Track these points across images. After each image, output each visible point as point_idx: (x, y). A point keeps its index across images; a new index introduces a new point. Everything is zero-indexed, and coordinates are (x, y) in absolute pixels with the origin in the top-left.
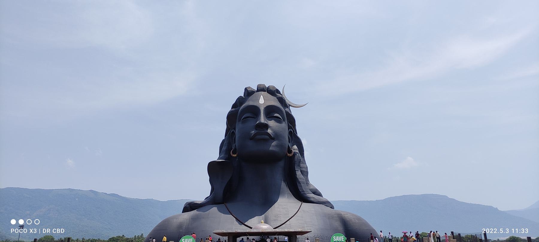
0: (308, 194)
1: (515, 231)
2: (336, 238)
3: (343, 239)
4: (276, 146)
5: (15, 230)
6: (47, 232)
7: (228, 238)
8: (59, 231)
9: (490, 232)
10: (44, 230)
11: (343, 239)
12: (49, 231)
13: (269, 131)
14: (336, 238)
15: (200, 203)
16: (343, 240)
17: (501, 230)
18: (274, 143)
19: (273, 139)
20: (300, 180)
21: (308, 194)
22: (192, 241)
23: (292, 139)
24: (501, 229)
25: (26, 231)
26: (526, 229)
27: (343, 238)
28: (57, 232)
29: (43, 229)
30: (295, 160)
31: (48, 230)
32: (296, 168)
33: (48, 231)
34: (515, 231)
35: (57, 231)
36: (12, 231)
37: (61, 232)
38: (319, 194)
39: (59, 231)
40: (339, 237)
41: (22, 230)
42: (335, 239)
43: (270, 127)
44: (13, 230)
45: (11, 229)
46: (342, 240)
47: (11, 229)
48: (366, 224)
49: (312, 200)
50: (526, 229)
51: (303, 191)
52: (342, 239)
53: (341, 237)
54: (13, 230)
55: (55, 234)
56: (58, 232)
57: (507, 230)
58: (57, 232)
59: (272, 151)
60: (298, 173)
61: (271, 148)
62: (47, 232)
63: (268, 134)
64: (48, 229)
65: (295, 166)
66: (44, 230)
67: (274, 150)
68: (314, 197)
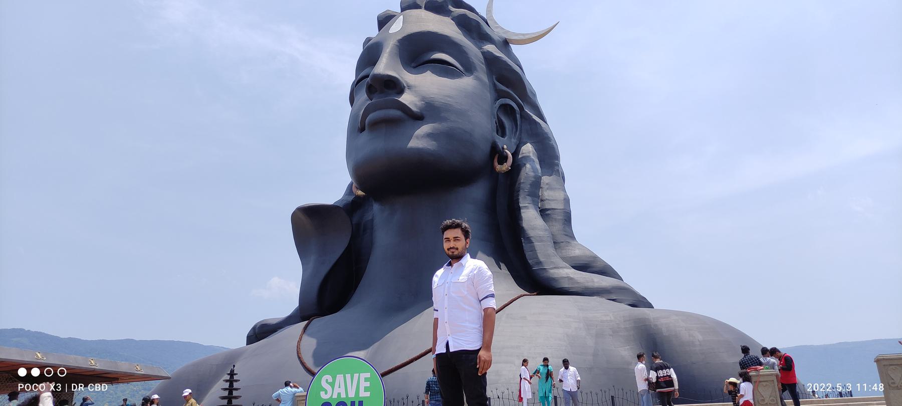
0: (552, 269)
1: (862, 387)
2: (332, 385)
3: (366, 389)
4: (430, 136)
5: (24, 386)
6: (79, 390)
7: (190, 394)
8: (881, 387)
9: (820, 389)
10: (74, 386)
11: (366, 389)
12: (82, 388)
13: (407, 99)
14: (332, 385)
15: (274, 322)
16: (368, 394)
17: (838, 387)
18: (425, 129)
19: (417, 118)
20: (531, 233)
21: (552, 271)
22: (368, 384)
23: (517, 128)
24: (838, 384)
25: (34, 388)
26: (827, 385)
27: (366, 380)
28: (95, 389)
29: (73, 385)
30: (521, 179)
31: (81, 386)
32: (521, 200)
33: (80, 387)
34: (862, 387)
35: (96, 387)
36: (19, 388)
37: (103, 390)
38: (606, 271)
39: (881, 387)
40: (348, 376)
41: (37, 385)
42: (328, 387)
43: (409, 87)
44: (21, 386)
45: (73, 385)
46: (363, 394)
47: (19, 385)
48: (535, 95)
49: (565, 285)
50: (827, 385)
51: (540, 263)
52: (364, 384)
53: (356, 375)
54: (21, 386)
55: (92, 392)
56: (98, 389)
57: (849, 386)
58: (96, 390)
59: (418, 151)
60: (530, 217)
61: (414, 143)
62: (79, 390)
63: (403, 108)
64: (80, 385)
65: (518, 195)
66: (74, 386)
67: (421, 146)
68: (572, 276)
